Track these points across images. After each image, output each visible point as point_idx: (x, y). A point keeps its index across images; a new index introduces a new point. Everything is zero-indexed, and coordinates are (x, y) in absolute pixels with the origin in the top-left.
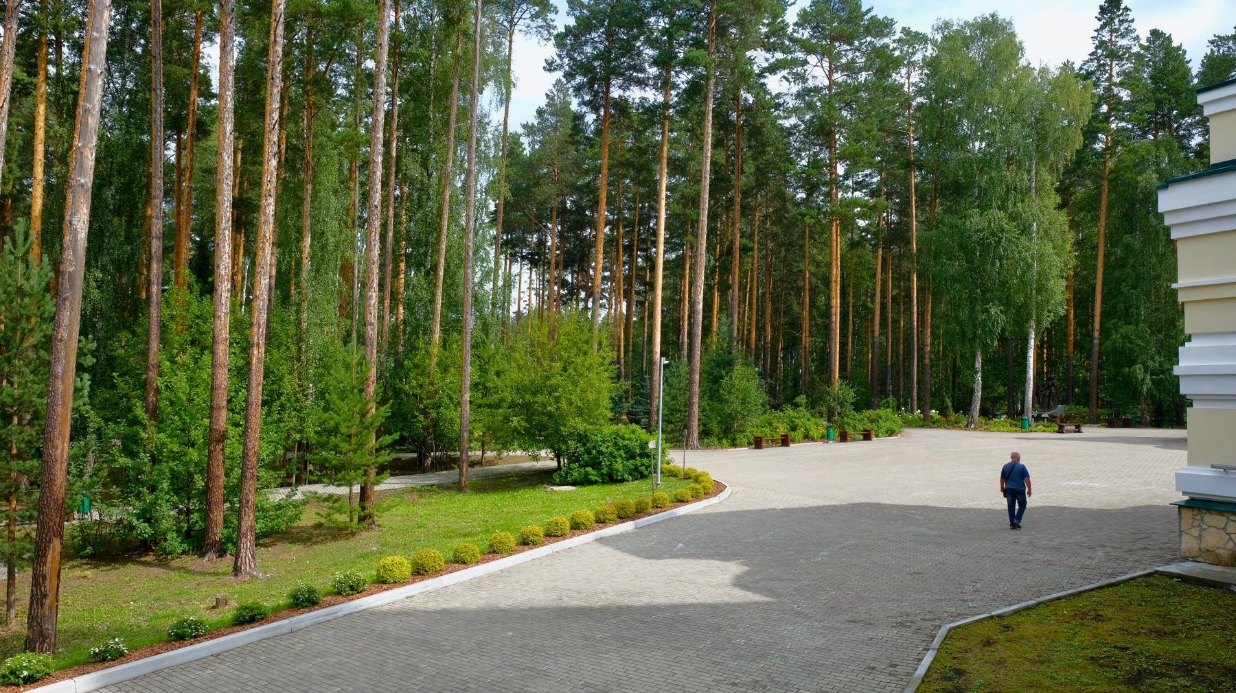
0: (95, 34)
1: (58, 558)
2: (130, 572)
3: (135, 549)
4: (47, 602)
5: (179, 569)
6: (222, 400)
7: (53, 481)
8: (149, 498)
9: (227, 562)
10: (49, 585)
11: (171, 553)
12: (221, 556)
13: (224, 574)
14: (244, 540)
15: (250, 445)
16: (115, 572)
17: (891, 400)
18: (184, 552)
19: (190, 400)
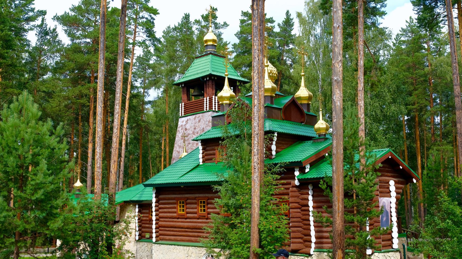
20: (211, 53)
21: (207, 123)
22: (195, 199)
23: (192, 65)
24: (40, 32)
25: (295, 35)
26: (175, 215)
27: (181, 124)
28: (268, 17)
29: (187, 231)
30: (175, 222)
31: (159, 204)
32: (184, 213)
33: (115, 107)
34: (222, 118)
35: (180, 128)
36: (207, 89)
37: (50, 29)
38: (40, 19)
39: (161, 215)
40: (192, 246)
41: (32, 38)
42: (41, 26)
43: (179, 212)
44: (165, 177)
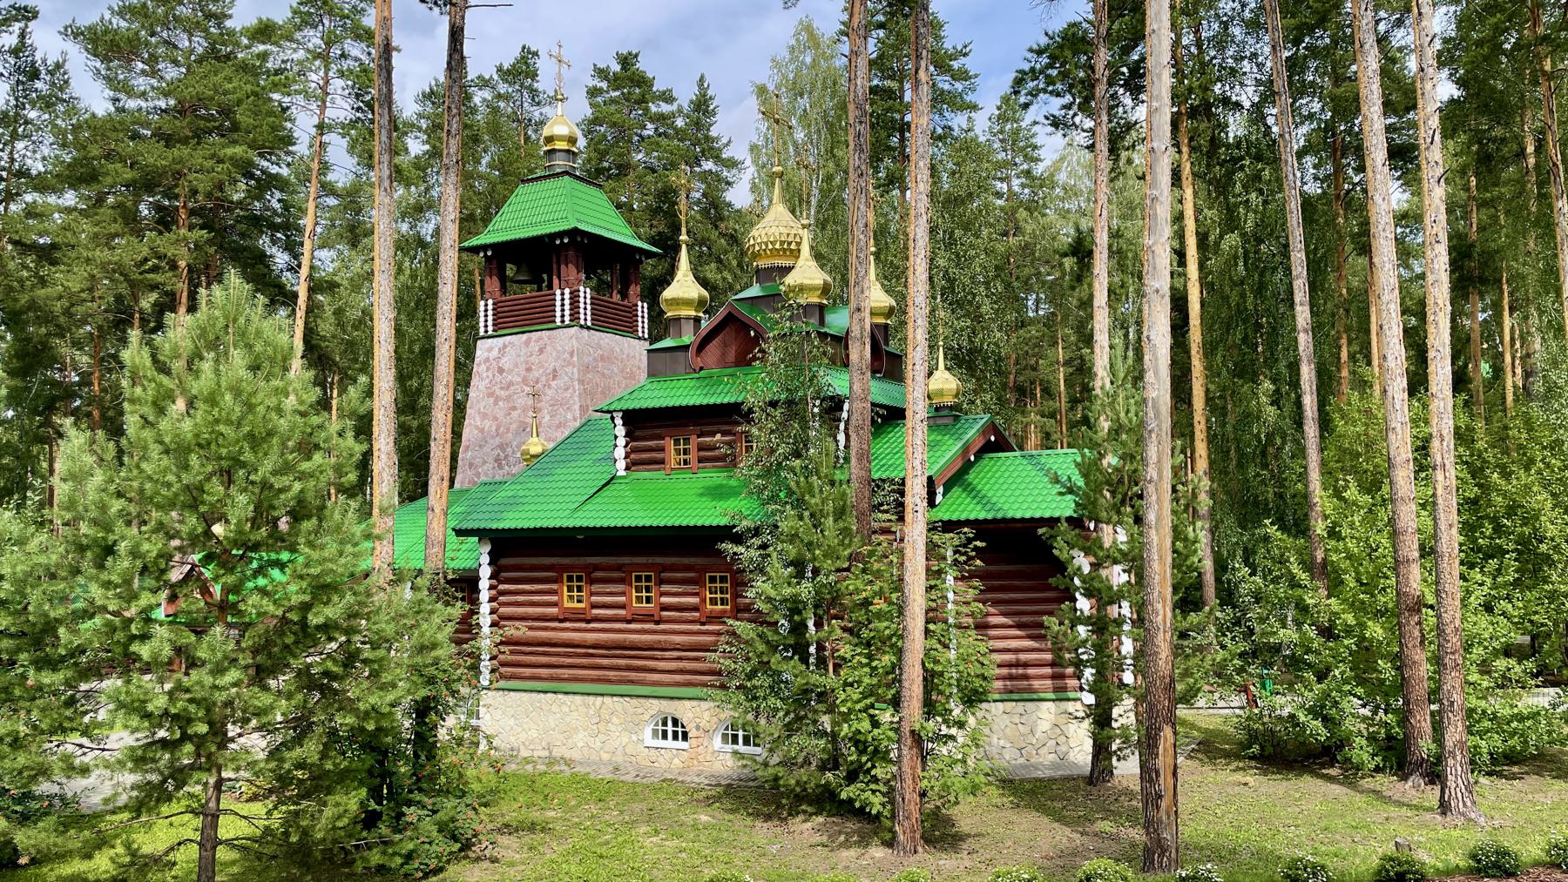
1: (1171, 752)
2: (1308, 784)
3: (1316, 757)
4: (1164, 804)
9: (1432, 795)
10: (1165, 782)
13: (1430, 809)
14: (1451, 762)
15: (1447, 617)
16: (1285, 783)
17: (1412, 368)
18: (1377, 769)
20: (566, 173)
21: (567, 355)
22: (619, 568)
25: (718, 139)
26: (555, 610)
28: (658, 87)
29: (592, 655)
31: (500, 582)
34: (681, 354)
35: (483, 367)
36: (563, 267)
37: (44, 61)
38: (17, 27)
43: (567, 604)
44: (527, 507)
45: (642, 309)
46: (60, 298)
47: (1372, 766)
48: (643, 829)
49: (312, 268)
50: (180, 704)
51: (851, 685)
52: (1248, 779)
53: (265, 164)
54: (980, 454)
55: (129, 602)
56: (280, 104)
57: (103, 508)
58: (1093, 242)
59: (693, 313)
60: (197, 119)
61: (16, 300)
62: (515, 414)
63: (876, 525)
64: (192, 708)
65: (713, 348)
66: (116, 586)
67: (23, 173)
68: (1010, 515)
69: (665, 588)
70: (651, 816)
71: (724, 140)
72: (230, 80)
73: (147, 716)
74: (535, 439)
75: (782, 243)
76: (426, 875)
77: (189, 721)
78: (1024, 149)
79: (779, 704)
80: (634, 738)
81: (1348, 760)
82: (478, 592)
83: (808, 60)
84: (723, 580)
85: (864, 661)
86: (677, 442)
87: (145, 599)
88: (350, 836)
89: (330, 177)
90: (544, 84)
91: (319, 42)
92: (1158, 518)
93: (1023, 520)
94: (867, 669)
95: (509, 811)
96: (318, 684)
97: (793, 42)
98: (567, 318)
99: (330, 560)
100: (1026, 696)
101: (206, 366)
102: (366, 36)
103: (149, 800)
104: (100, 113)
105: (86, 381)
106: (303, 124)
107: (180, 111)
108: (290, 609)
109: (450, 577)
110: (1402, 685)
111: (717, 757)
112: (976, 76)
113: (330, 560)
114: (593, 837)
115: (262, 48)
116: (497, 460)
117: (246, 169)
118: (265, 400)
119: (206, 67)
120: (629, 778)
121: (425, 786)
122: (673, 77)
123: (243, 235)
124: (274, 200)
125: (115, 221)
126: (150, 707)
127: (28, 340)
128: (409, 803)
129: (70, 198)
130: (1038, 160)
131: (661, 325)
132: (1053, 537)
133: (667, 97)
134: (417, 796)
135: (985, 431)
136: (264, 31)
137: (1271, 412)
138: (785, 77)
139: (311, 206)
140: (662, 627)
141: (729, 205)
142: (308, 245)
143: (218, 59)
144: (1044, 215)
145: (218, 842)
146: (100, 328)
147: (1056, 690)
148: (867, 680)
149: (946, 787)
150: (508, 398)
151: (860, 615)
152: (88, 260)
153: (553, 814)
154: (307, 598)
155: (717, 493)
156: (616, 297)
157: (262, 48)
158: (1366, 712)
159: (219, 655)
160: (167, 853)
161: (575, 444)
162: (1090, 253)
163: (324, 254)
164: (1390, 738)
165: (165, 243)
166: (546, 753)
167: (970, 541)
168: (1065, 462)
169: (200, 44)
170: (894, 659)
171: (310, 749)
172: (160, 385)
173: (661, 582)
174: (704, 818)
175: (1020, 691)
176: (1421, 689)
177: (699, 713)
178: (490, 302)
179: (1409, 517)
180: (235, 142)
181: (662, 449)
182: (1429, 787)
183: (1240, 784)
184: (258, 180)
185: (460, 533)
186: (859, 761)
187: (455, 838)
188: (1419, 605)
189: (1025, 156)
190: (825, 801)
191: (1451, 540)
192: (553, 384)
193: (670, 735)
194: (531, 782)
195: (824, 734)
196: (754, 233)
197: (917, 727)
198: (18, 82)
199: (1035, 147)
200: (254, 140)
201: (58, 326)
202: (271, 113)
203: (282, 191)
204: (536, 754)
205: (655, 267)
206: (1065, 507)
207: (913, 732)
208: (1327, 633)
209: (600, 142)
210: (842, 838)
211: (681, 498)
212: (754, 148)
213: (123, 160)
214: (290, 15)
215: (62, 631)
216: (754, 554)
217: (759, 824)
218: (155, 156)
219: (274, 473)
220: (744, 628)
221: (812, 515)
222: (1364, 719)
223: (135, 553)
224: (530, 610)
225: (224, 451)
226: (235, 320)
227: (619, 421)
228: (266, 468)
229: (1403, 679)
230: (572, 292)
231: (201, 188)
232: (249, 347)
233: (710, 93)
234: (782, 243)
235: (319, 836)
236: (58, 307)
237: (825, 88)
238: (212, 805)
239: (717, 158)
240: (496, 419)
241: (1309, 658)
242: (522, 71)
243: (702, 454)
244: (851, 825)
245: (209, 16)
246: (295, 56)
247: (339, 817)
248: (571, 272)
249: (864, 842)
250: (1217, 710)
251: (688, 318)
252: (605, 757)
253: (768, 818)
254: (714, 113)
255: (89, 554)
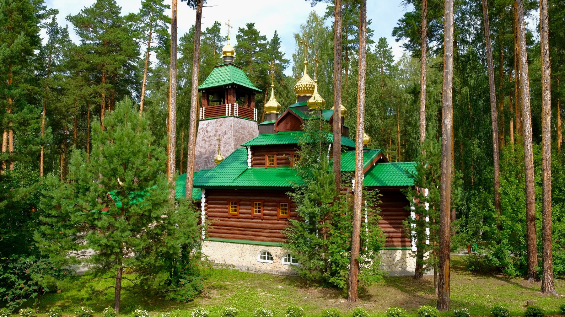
0: (448, 39)
1: (448, 269)
3: (494, 271)
4: (445, 287)
5: (514, 283)
6: (532, 198)
7: (444, 234)
8: (497, 247)
9: (538, 285)
10: (445, 279)
11: (510, 275)
12: (537, 281)
13: (537, 290)
14: (546, 274)
16: (484, 280)
18: (517, 276)
19: (517, 199)
20: (230, 64)
22: (249, 201)
23: (212, 73)
24: (52, 31)
25: (281, 53)
26: (226, 214)
27: (202, 126)
28: (261, 34)
30: (227, 221)
31: (208, 204)
32: (236, 213)
33: (191, 114)
34: (271, 126)
35: (201, 130)
37: (61, 28)
38: (52, 16)
39: (209, 214)
40: (247, 244)
41: (44, 36)
42: (51, 25)
43: (231, 212)
45: (255, 111)
46: (64, 106)
47: (515, 274)
48: (259, 290)
49: (145, 97)
50: (111, 242)
51: (334, 243)
52: (471, 278)
53: (130, 62)
54: (377, 163)
55: (94, 207)
56: (135, 41)
57: (86, 176)
58: (421, 89)
59: (275, 112)
60: (110, 47)
61: (51, 107)
62: (212, 147)
63: (342, 188)
64: (114, 243)
65: (282, 124)
66: (90, 202)
67: (54, 65)
68: (389, 185)
69: (265, 208)
70: (261, 285)
71: (283, 53)
72: (119, 34)
73: (100, 245)
74: (219, 155)
75: (307, 88)
76: (187, 302)
77: (113, 248)
78: (388, 57)
79: (307, 249)
80: (254, 258)
81: (507, 272)
82: (201, 207)
83: (314, 25)
84: (286, 205)
85: (339, 235)
86: (269, 157)
87: (99, 206)
88: (164, 288)
89: (150, 66)
90: (223, 34)
91: (148, 21)
92: (446, 187)
93: (393, 187)
94: (339, 238)
95: (213, 281)
96: (154, 236)
97: (309, 19)
98: (230, 114)
99: (159, 195)
100: (392, 248)
101: (119, 128)
102: (165, 19)
103: (98, 273)
104: (78, 45)
105: (71, 133)
106: (143, 48)
107: (103, 45)
108: (145, 211)
109: (195, 202)
110: (527, 247)
111: (282, 265)
112: (373, 31)
113: (159, 195)
114: (242, 291)
115: (130, 23)
116: (206, 162)
117: (124, 63)
118: (137, 141)
119: (112, 30)
120: (253, 272)
121: (186, 272)
122: (266, 31)
123: (122, 86)
124: (133, 74)
125: (82, 81)
126: (101, 243)
127: (54, 120)
128: (181, 278)
129: (68, 73)
130: (393, 61)
131: (262, 116)
132: (407, 193)
133: (264, 38)
134: (183, 275)
135: (379, 155)
136: (131, 17)
137: (477, 150)
138: (305, 31)
139: (145, 76)
140: (264, 221)
141: (284, 75)
142: (143, 89)
143: (116, 27)
144: (394, 80)
145: (121, 288)
146: (77, 116)
147: (402, 246)
148: (339, 242)
149: (367, 279)
150: (209, 141)
151: (336, 219)
152: (74, 94)
153: (227, 283)
154: (151, 208)
155: (283, 175)
156: (246, 107)
157: (130, 23)
158: (512, 255)
159: (123, 226)
160: (104, 290)
161: (233, 157)
162: (419, 92)
163: (148, 92)
164: (521, 265)
165: (98, 88)
166: (224, 263)
167: (377, 194)
168: (411, 166)
169: (110, 22)
170: (349, 234)
171: (151, 259)
172: (103, 134)
173: (264, 206)
174: (280, 287)
175: (390, 246)
176: (534, 247)
177: (275, 251)
178: (204, 108)
179: (532, 188)
180: (120, 54)
181: (264, 160)
182: (536, 282)
183: (468, 280)
184: (128, 67)
185: (195, 187)
186: (336, 269)
187: (196, 290)
188: (534, 219)
189: (388, 59)
190: (324, 283)
191: (548, 196)
192: (225, 136)
193: (266, 258)
194: (221, 272)
195: (322, 259)
196: (297, 84)
197: (357, 258)
198: (52, 35)
199: (392, 56)
200: (127, 54)
201: (64, 115)
202: (133, 45)
203: (135, 71)
204: (220, 262)
205: (258, 96)
206: (410, 182)
207: (356, 260)
208: (500, 228)
209: (240, 54)
210: (329, 295)
211: (271, 176)
212: (294, 56)
213: (85, 61)
214: (139, 12)
215: (72, 216)
216: (299, 196)
217: (299, 289)
218: (95, 59)
219: (141, 165)
220: (295, 222)
221: (320, 184)
222: (513, 258)
223: (96, 191)
224: (219, 214)
225: (124, 157)
226: (127, 113)
227: (249, 150)
228: (138, 162)
229: (528, 244)
230: (232, 105)
231: (110, 70)
232: (132, 122)
233: (278, 37)
234: (307, 88)
235: (154, 287)
236: (64, 109)
237: (319, 34)
238: (119, 275)
239: (280, 59)
240: (205, 148)
241: (494, 236)
242: (215, 29)
243: (278, 161)
244: (331, 291)
245: (113, 13)
246: (141, 26)
247: (161, 282)
248: (231, 98)
249: (336, 297)
250: (460, 255)
251: (274, 114)
252: (244, 265)
253: (302, 287)
254: (279, 44)
255: (81, 191)
